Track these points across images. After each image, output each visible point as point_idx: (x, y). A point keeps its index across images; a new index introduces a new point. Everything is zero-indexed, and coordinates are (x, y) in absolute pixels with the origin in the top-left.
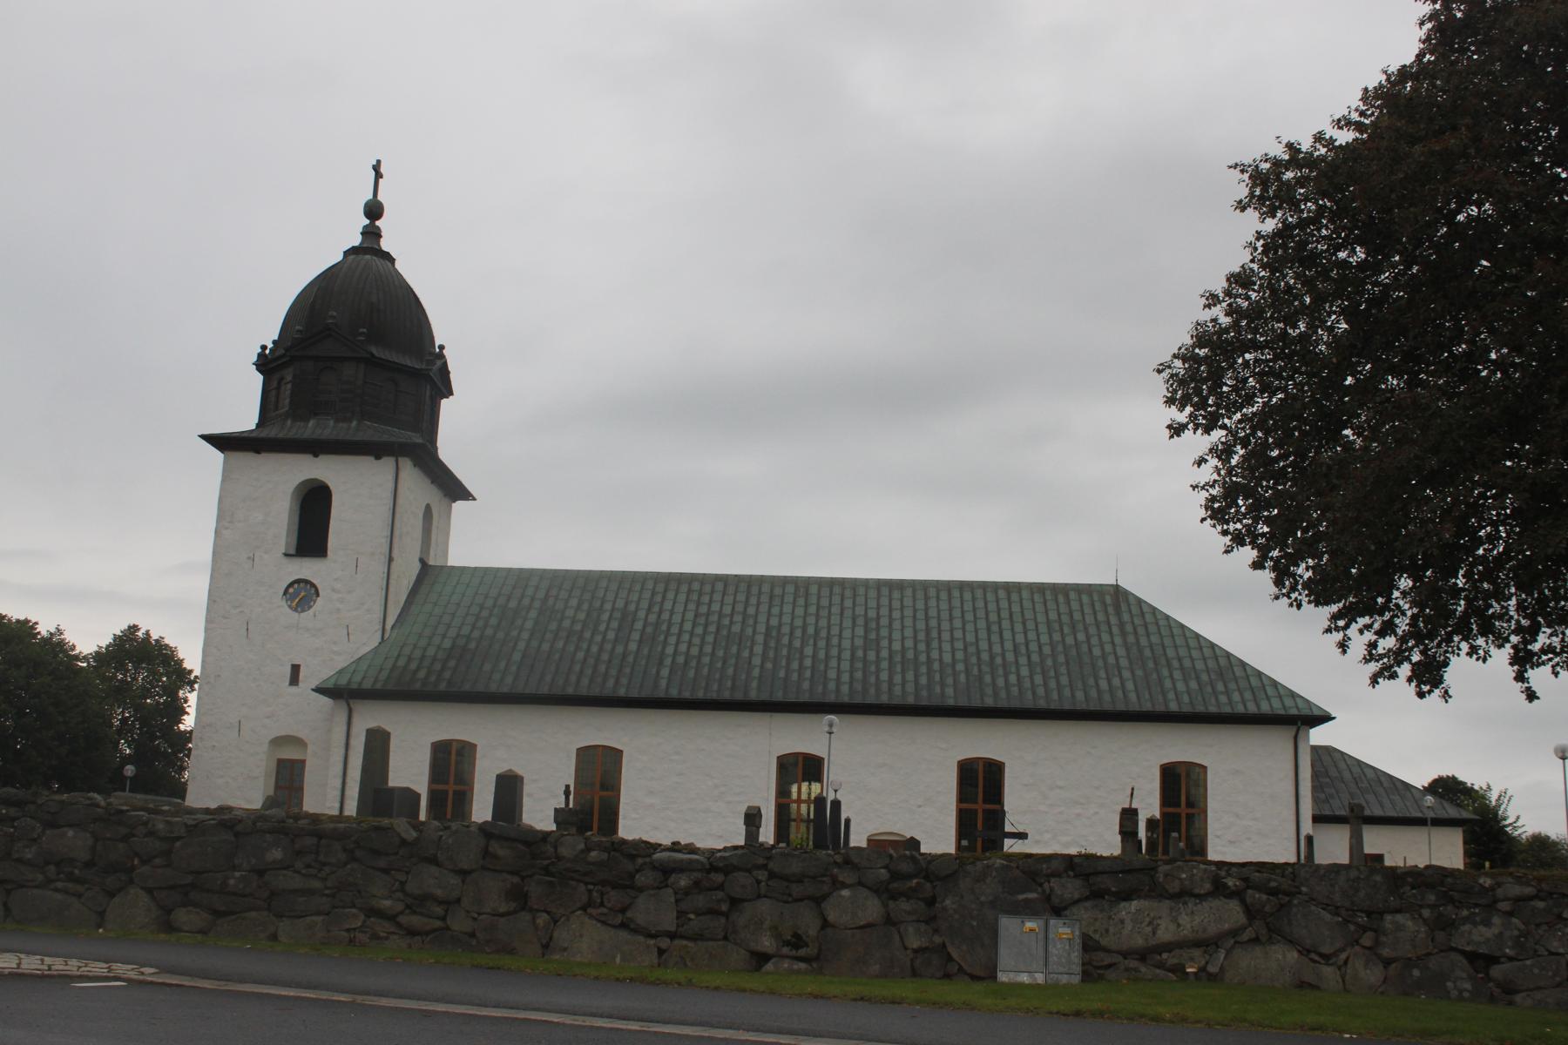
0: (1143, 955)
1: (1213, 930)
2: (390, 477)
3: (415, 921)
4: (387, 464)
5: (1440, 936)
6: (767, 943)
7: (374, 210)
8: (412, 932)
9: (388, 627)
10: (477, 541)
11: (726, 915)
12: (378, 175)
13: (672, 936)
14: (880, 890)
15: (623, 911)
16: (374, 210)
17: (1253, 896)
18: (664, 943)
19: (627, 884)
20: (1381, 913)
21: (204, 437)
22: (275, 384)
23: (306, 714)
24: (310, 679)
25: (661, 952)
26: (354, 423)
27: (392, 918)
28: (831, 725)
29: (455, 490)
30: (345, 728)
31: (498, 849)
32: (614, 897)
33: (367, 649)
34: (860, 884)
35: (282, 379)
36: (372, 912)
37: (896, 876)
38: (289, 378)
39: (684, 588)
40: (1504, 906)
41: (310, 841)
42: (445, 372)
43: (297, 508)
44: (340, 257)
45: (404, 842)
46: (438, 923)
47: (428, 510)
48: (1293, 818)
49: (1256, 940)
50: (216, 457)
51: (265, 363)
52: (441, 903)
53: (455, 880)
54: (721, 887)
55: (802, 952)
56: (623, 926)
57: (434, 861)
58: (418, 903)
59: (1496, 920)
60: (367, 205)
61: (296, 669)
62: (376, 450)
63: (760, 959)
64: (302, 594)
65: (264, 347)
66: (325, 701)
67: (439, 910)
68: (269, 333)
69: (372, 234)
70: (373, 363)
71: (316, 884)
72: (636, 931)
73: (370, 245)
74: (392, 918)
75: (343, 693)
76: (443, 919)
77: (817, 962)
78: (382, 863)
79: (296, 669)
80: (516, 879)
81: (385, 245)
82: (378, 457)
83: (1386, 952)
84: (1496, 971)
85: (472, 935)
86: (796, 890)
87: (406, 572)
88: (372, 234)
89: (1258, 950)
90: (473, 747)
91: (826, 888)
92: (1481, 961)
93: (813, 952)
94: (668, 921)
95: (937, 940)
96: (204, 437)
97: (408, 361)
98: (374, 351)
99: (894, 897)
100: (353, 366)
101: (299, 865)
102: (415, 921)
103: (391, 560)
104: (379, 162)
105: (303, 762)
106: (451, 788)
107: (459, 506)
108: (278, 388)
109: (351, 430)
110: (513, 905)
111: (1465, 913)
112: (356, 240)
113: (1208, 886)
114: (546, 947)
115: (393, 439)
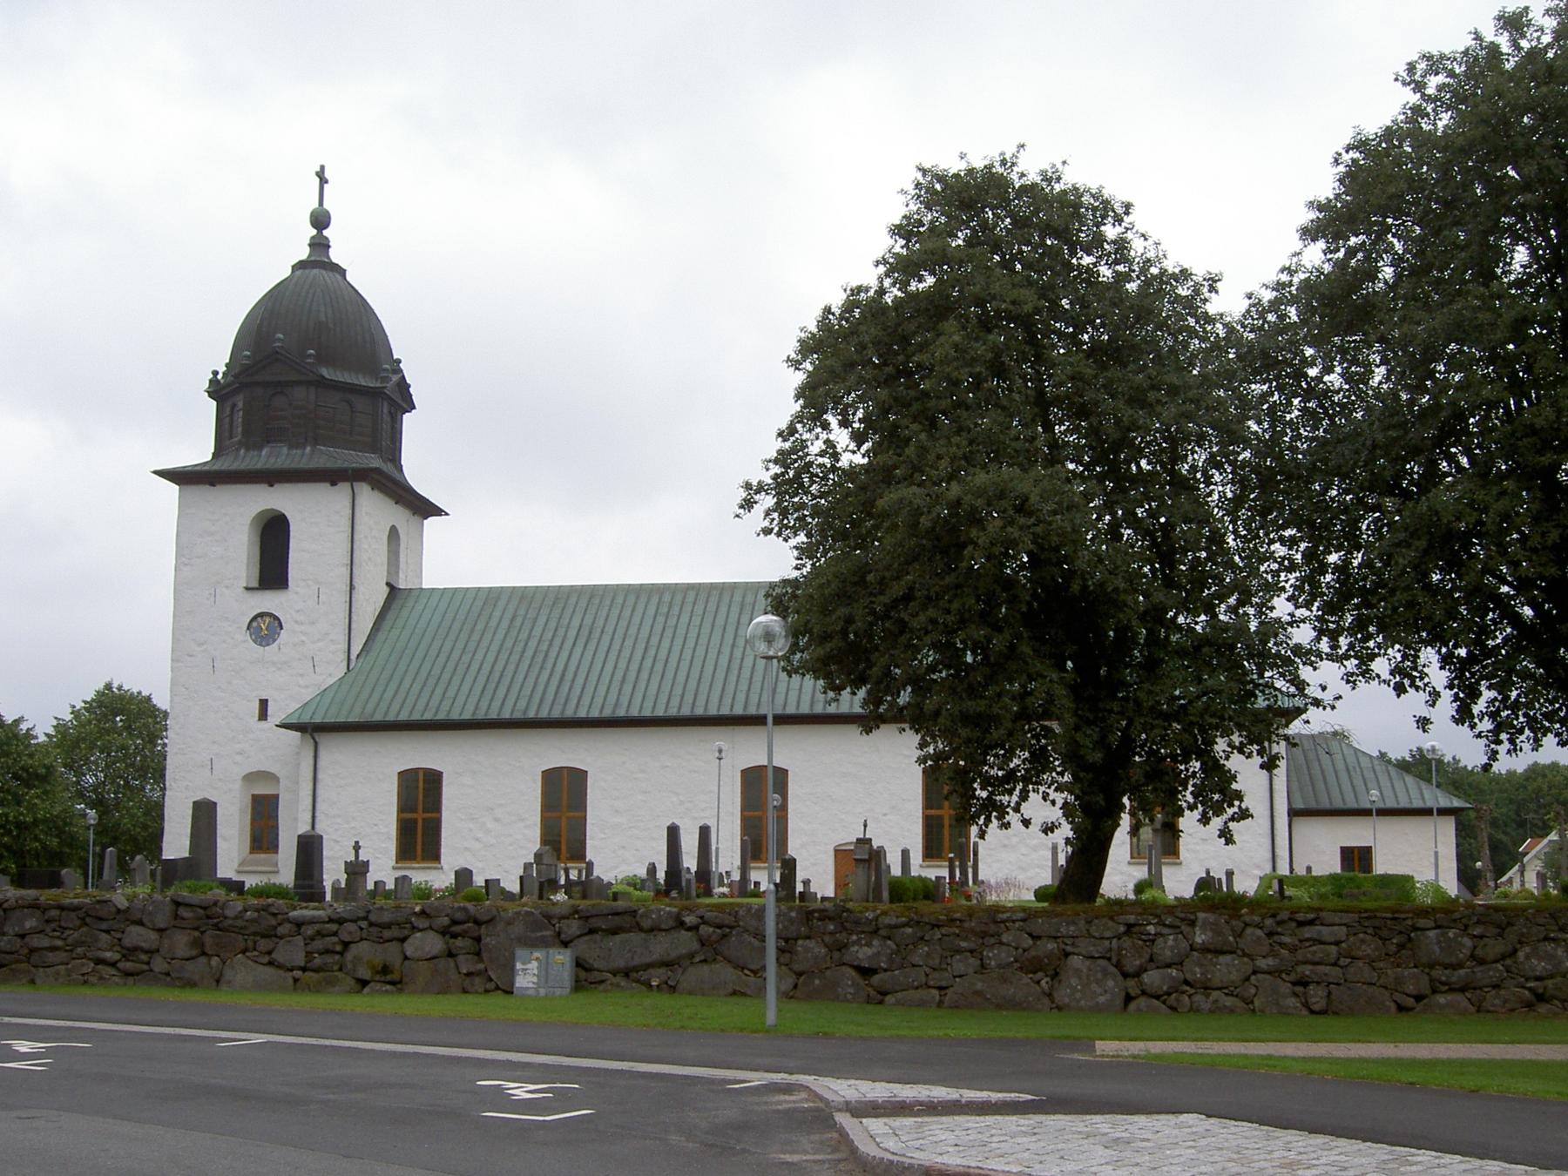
0: (627, 973)
1: (674, 955)
2: (348, 504)
3: (128, 966)
4: (344, 489)
5: (836, 955)
6: (365, 974)
7: (320, 220)
8: (128, 974)
9: (353, 657)
10: (450, 558)
11: (341, 954)
12: (323, 181)
13: (304, 969)
14: (444, 932)
15: (269, 953)
16: (320, 220)
17: (704, 930)
18: (298, 973)
19: (270, 934)
20: (796, 940)
21: (156, 472)
22: (228, 411)
23: (276, 749)
24: (276, 714)
25: (296, 980)
26: (308, 449)
27: (113, 964)
28: (720, 751)
29: (425, 509)
30: (311, 762)
31: (183, 912)
32: (264, 944)
33: (331, 681)
34: (431, 928)
35: (234, 406)
36: (99, 961)
37: (454, 922)
38: (240, 405)
39: (655, 600)
40: (883, 932)
41: (54, 913)
42: (403, 387)
43: (257, 539)
44: (288, 272)
45: (119, 911)
46: (145, 967)
47: (393, 534)
48: (1268, 813)
49: (704, 961)
50: (174, 488)
51: (217, 390)
52: (147, 952)
53: (153, 936)
54: (335, 934)
55: (389, 978)
56: (271, 963)
57: (140, 923)
58: (130, 952)
59: (875, 942)
60: (312, 214)
61: (264, 704)
62: (332, 477)
63: (363, 983)
64: (265, 628)
65: (215, 373)
66: (295, 735)
67: (144, 957)
68: (219, 358)
69: (320, 245)
70: (323, 384)
71: (59, 943)
72: (280, 966)
73: (319, 256)
74: (113, 964)
75: (313, 730)
76: (148, 963)
77: (398, 985)
78: (104, 926)
79: (264, 704)
80: (196, 934)
81: (335, 255)
82: (334, 484)
83: (797, 967)
84: (876, 979)
85: (168, 974)
86: (387, 934)
87: (372, 597)
88: (320, 245)
89: (706, 967)
90: (440, 774)
91: (406, 932)
92: (866, 972)
93: (390, 978)
94: (300, 960)
95: (481, 966)
96: (156, 472)
97: (363, 381)
98: (325, 372)
99: (455, 936)
100: (309, 394)
101: (48, 930)
102: (128, 966)
103: (352, 587)
104: (322, 167)
105: (277, 797)
106: (420, 816)
107: (431, 523)
108: (232, 415)
109: (306, 458)
110: (194, 953)
111: (854, 937)
112: (304, 253)
113: (671, 923)
114: (218, 981)
115: (346, 465)
